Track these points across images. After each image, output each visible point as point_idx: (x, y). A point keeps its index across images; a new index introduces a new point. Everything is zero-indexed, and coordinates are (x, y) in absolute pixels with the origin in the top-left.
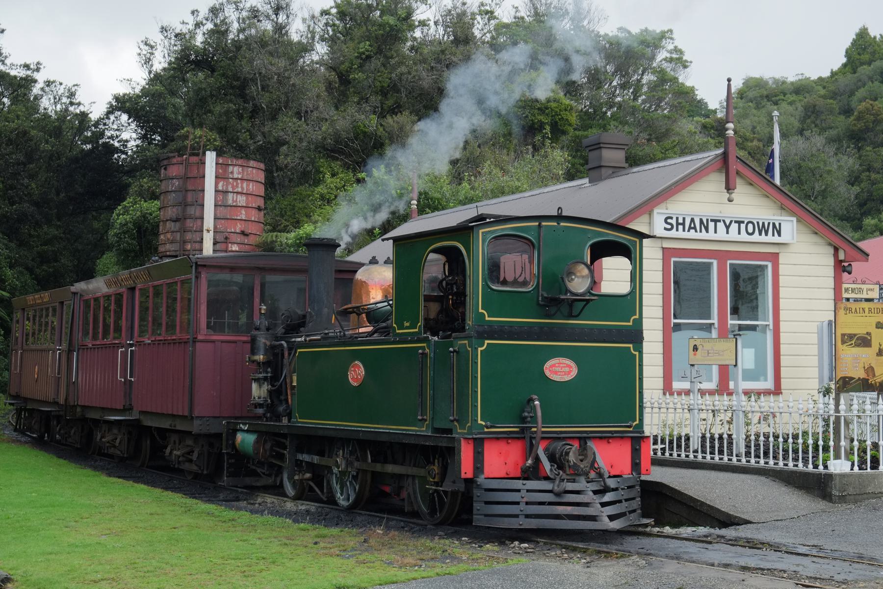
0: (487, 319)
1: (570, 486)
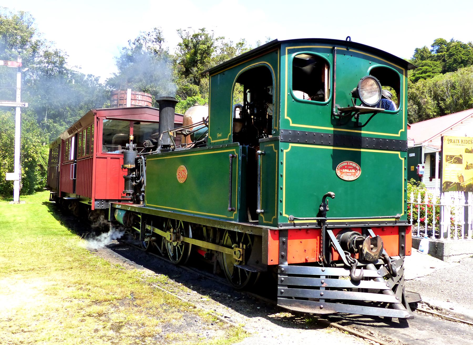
0: (291, 125)
1: (366, 273)
